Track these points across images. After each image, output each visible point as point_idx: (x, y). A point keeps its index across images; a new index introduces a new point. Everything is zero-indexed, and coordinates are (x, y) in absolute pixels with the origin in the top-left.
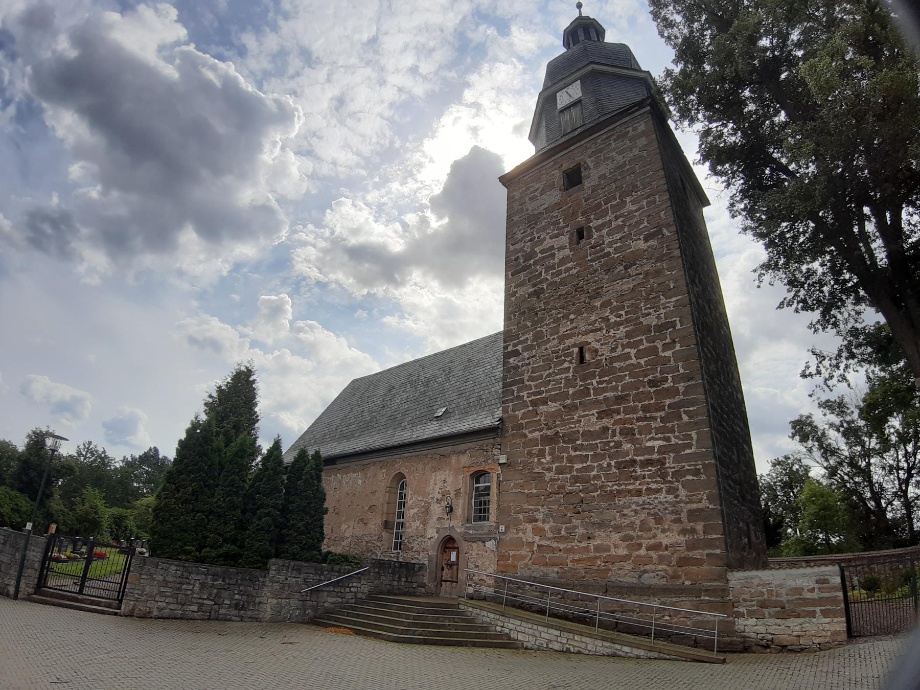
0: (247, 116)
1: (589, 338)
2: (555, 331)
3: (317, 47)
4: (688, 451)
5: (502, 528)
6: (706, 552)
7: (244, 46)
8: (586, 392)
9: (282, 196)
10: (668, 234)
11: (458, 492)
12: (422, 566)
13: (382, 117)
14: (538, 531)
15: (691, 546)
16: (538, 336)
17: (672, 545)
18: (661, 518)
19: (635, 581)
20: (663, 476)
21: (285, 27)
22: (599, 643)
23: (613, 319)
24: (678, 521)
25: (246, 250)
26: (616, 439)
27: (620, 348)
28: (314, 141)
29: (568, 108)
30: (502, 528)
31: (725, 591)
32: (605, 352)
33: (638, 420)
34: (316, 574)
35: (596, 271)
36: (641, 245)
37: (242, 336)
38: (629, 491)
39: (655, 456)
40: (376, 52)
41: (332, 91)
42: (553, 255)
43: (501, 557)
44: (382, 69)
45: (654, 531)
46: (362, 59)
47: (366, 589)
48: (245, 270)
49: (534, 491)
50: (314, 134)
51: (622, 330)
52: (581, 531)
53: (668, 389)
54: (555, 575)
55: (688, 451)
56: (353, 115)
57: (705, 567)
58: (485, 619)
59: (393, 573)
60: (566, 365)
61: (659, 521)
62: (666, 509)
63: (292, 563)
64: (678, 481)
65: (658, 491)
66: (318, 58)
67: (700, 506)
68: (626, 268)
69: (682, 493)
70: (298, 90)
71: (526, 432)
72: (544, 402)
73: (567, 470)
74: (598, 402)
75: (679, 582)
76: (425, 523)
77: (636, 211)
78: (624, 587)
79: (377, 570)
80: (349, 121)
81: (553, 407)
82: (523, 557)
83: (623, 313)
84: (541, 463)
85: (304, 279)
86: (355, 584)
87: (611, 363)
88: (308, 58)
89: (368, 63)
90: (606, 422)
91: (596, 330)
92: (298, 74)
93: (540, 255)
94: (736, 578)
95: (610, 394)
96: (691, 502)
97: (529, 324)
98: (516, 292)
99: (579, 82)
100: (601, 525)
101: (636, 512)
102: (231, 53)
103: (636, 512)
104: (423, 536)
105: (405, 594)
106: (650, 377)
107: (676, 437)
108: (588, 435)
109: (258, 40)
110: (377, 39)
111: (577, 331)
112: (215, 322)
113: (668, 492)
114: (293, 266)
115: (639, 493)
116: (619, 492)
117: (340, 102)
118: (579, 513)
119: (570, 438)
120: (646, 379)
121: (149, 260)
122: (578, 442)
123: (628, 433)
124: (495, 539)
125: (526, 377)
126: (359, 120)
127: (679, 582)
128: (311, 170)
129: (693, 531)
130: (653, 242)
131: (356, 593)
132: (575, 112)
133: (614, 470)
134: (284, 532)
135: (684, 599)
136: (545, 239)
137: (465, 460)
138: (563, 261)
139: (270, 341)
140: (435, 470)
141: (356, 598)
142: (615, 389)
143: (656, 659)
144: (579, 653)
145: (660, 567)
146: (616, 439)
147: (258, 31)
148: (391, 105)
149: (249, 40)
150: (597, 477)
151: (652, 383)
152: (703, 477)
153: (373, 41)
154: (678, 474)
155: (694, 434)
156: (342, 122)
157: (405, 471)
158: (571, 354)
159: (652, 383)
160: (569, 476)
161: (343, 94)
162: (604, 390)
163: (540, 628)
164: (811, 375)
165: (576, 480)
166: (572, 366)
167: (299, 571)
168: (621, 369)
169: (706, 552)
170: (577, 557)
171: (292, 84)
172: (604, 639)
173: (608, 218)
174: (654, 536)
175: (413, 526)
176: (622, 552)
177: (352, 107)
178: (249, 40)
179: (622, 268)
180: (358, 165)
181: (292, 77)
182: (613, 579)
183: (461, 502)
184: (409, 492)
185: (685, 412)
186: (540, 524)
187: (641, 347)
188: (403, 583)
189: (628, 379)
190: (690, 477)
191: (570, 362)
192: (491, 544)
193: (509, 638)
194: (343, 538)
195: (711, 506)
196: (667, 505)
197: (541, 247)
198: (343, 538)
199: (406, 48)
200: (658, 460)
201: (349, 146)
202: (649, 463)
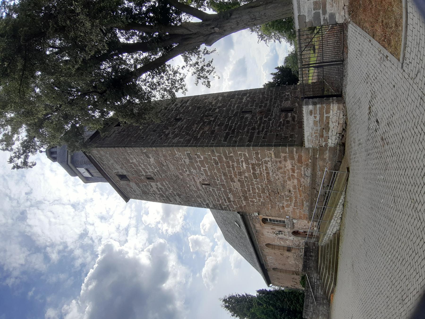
0: (111, 266)
1: (198, 182)
2: (196, 192)
3: (79, 231)
4: (247, 155)
5: (287, 217)
6: (295, 153)
7: (81, 265)
8: (223, 185)
9: (147, 240)
10: (145, 150)
11: (272, 229)
12: (306, 243)
13: (107, 198)
14: (288, 206)
15: (292, 158)
16: (198, 197)
17: (292, 165)
18: (279, 167)
19: (309, 179)
20: (259, 165)
21: (71, 246)
22: (337, 209)
23: (188, 173)
24: (280, 162)
25: (172, 261)
26: (243, 178)
27: (201, 172)
28: (121, 228)
29: (90, 173)
30: (287, 217)
31: (314, 149)
32: (204, 177)
33: (234, 170)
34: (309, 298)
35: (166, 176)
36: (152, 160)
37: (210, 255)
38: (267, 176)
39: (250, 166)
40: (78, 204)
41: (97, 222)
42: (160, 188)
43: (300, 218)
44: (86, 201)
45: (285, 170)
46: (82, 211)
47: (315, 275)
48: (181, 254)
49: (270, 205)
50: (118, 229)
51: (192, 170)
52: (287, 193)
53: (219, 159)
54: (307, 203)
55: (247, 155)
56: (108, 212)
57: (303, 154)
58: (327, 239)
59: (309, 259)
60: (211, 190)
61: (280, 168)
62: (275, 165)
63: (304, 309)
64: (261, 160)
65: (266, 167)
66: (84, 230)
67: (273, 153)
68: (164, 166)
69: (267, 159)
70: (99, 238)
71: (243, 205)
72: (229, 199)
73: (259, 194)
74: (227, 182)
75: (310, 164)
76: (287, 240)
77: (136, 159)
78: (312, 183)
79: (307, 269)
80: (111, 214)
81: (230, 196)
82: (300, 212)
83: (185, 169)
84: (257, 202)
85: (183, 227)
86: (313, 280)
87: (208, 176)
88: (84, 235)
89: (84, 208)
90: (236, 180)
91: (194, 179)
92: (91, 239)
93: (161, 192)
94: (307, 144)
95: (223, 178)
96: (271, 157)
97: (193, 199)
98: (179, 202)
99: (78, 168)
100: (284, 187)
101: (277, 175)
102: (85, 270)
103: (277, 175)
104: (293, 241)
105: (318, 253)
106: (214, 164)
107: (241, 158)
108: (242, 186)
109: (78, 259)
110: (72, 204)
111: (195, 185)
112: (204, 270)
113: (267, 164)
114: (178, 232)
115: (268, 173)
116: (267, 179)
117: (102, 218)
118: (278, 193)
119: (244, 192)
120: (215, 165)
121: (179, 304)
122: (246, 190)
123: (240, 174)
124: (292, 220)
125: (218, 203)
126: (110, 209)
127: (310, 164)
128: (134, 228)
129: (285, 157)
130: (150, 156)
131: (317, 280)
132: (91, 171)
133: (258, 180)
134: (291, 310)
135: (318, 164)
136: (153, 190)
137: (257, 225)
138: (163, 185)
139: (211, 244)
140: (263, 234)
141: (319, 280)
142: (220, 176)
143: (345, 193)
144: (342, 215)
145: (303, 169)
146: (243, 178)
147: (74, 259)
148: (102, 194)
149: (78, 263)
150: (262, 186)
151: (217, 163)
152: (259, 151)
153: (74, 206)
154: (258, 159)
155: (239, 153)
156: (111, 217)
157: (264, 244)
158: (206, 188)
159: (217, 163)
160: (262, 194)
161: (99, 217)
162: (221, 179)
163: (331, 224)
164: (209, 82)
165: (263, 192)
166: (211, 188)
167: (307, 306)
168: (211, 173)
169: (295, 153)
170: (299, 195)
171: (96, 241)
172: (336, 207)
173: (141, 169)
174: (288, 170)
175: (288, 243)
176: (296, 181)
177: (104, 213)
178: (78, 263)
179: (164, 167)
180: (130, 207)
181: (93, 241)
182: (308, 185)
183: (277, 228)
184: (273, 243)
185: (229, 154)
186: (284, 205)
187: (200, 165)
188: (313, 254)
189: (216, 171)
190: (259, 156)
191: (210, 188)
192: (295, 221)
193: (336, 233)
194: (295, 263)
195: (273, 150)
196: (273, 165)
197: (157, 192)
198: (295, 263)
199: (76, 191)
200: (252, 165)
201: (122, 212)
202: (254, 169)
